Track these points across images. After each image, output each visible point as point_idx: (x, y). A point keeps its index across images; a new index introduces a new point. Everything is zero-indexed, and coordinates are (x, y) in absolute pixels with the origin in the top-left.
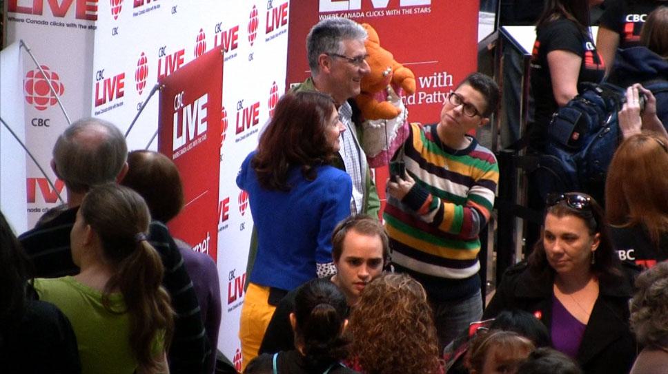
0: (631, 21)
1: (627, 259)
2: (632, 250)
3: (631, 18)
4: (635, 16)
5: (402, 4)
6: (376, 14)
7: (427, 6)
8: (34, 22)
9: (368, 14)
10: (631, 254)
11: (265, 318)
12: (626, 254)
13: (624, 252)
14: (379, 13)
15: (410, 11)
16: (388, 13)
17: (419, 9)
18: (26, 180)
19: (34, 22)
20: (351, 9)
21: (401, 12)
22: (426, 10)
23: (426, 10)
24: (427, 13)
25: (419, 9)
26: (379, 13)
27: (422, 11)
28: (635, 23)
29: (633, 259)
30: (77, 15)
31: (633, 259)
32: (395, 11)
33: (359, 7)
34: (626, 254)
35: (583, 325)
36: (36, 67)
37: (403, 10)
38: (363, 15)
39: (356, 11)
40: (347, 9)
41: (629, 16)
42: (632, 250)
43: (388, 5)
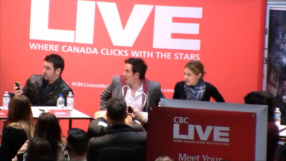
0: (177, 122)
1: (184, 122)
2: (188, 118)
3: (177, 120)
4: (180, 118)
5: (155, 45)
6: (117, 53)
9: (105, 52)
10: (187, 120)
13: (182, 118)
14: (120, 53)
15: (168, 56)
16: (208, 143)
18: (220, 138)
20: (76, 42)
21: (155, 55)
25: (181, 54)
29: (187, 123)
31: (187, 123)
32: (145, 52)
33: (90, 41)
34: (183, 120)
35: (7, 110)
36: (89, 120)
37: (158, 53)
39: (191, 140)
40: (73, 41)
41: (197, 141)
42: (188, 118)
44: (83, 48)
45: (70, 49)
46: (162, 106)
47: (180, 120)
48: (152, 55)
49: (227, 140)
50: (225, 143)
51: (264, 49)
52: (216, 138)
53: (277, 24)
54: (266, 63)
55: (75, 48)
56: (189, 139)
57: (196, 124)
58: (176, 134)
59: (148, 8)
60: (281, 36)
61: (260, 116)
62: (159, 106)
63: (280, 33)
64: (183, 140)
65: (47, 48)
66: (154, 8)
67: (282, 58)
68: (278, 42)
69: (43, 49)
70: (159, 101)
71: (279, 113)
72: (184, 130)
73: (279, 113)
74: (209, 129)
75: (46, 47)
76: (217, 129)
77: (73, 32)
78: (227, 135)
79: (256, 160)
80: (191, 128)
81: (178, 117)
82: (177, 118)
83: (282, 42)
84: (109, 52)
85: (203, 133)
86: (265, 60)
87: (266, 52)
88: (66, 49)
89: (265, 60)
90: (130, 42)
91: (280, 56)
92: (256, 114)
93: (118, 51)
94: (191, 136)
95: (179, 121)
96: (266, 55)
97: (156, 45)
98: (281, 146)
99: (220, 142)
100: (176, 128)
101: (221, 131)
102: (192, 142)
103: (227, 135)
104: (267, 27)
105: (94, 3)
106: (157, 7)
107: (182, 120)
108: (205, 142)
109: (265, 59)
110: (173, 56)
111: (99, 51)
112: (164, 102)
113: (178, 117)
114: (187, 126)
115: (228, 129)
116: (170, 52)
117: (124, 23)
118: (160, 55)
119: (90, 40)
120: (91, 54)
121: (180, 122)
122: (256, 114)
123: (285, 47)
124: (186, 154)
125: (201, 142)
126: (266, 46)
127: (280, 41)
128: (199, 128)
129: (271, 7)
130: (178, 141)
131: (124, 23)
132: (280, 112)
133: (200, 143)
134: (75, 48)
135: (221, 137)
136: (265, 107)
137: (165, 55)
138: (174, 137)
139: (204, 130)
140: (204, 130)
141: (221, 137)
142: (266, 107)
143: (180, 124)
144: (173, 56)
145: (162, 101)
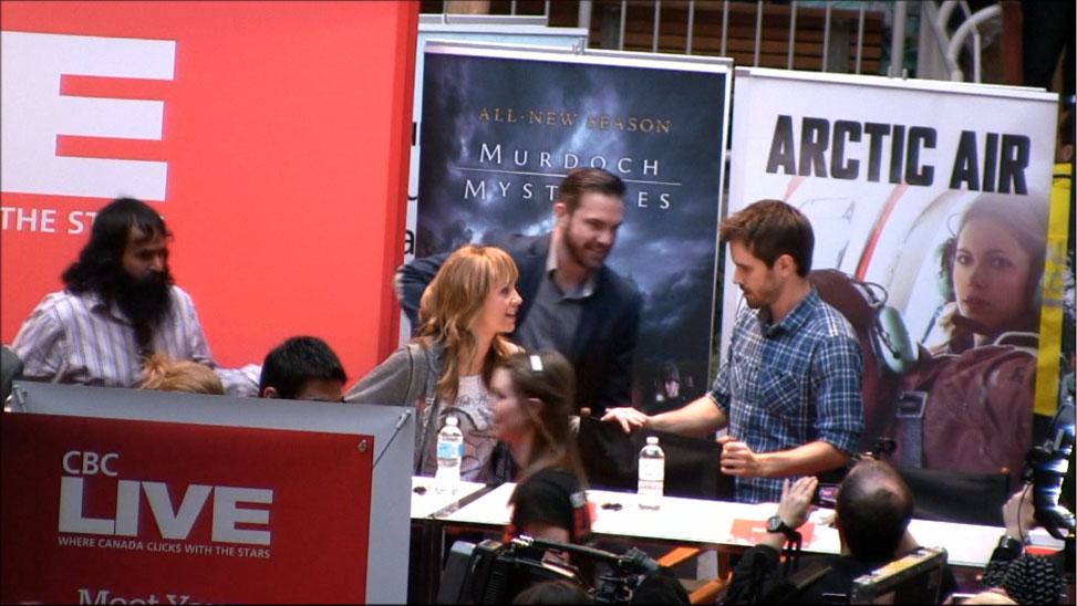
0: (77, 472)
2: (116, 456)
3: (77, 463)
4: (87, 455)
6: (167, 547)
7: (265, 548)
8: (732, 92)
9: (152, 546)
10: (111, 464)
11: (742, 306)
12: (99, 463)
13: (96, 456)
15: (231, 552)
16: (190, 549)
17: (247, 550)
19: (732, 92)
20: (117, 533)
22: (261, 553)
23: (261, 553)
24: (263, 560)
25: (247, 550)
26: (171, 547)
27: (254, 553)
28: (87, 478)
29: (115, 474)
30: (61, 90)
32: (201, 547)
33: (135, 533)
34: (99, 463)
37: (218, 548)
38: (140, 546)
39: (128, 539)
40: (112, 533)
43: (189, 536)
44: (124, 542)
45: (108, 544)
46: (19, 411)
47: (86, 463)
48: (210, 550)
49: (264, 538)
50: (258, 547)
51: (403, 197)
52: (223, 531)
53: (454, 108)
54: (411, 251)
55: (115, 542)
56: (120, 532)
57: (147, 480)
58: (72, 517)
59: (206, 490)
60: (465, 152)
61: (382, 455)
62: (8, 410)
63: (463, 141)
64: (97, 537)
65: (49, 225)
66: (213, 491)
67: (470, 232)
68: (455, 172)
69: (33, 228)
70: (9, 390)
71: (455, 435)
72: (100, 501)
73: (457, 435)
74: (196, 495)
75: (45, 221)
76: (227, 497)
77: (113, 521)
78: (263, 517)
79: (368, 602)
80: (128, 492)
81: (78, 453)
82: (73, 456)
83: (469, 175)
84: (158, 547)
85: (172, 513)
86: (407, 241)
87: (412, 207)
88: (104, 544)
89: (407, 241)
90: (183, 533)
91: (464, 224)
92: (370, 440)
93: (82, 456)
94: (127, 521)
95: (81, 469)
96: (411, 224)
97: (217, 536)
98: (462, 557)
99: (237, 546)
100: (72, 492)
101: (76, 86)
102: (132, 545)
103: (263, 517)
104: (417, 117)
105: (138, 483)
106: (217, 489)
107: (94, 462)
108: (178, 546)
109: (408, 237)
110: (236, 553)
111: (145, 546)
112: (25, 394)
113: (78, 453)
114: (113, 483)
115: (266, 496)
116: (51, 208)
117: (176, 513)
118: (13, 217)
119: (133, 532)
120: (134, 550)
121: (85, 471)
122: (370, 440)
123: (480, 194)
124: (106, 590)
125: (166, 544)
126: (413, 190)
127: (463, 171)
128: (158, 492)
129: (429, 43)
130: (77, 542)
131: (176, 513)
132: (458, 431)
133: (162, 547)
134: (115, 542)
135: (240, 526)
136: (404, 416)
137: (33, 220)
138: (64, 527)
139: (177, 500)
140: (177, 500)
141: (240, 526)
142: (409, 415)
143: (87, 478)
144: (236, 553)
145: (19, 392)
